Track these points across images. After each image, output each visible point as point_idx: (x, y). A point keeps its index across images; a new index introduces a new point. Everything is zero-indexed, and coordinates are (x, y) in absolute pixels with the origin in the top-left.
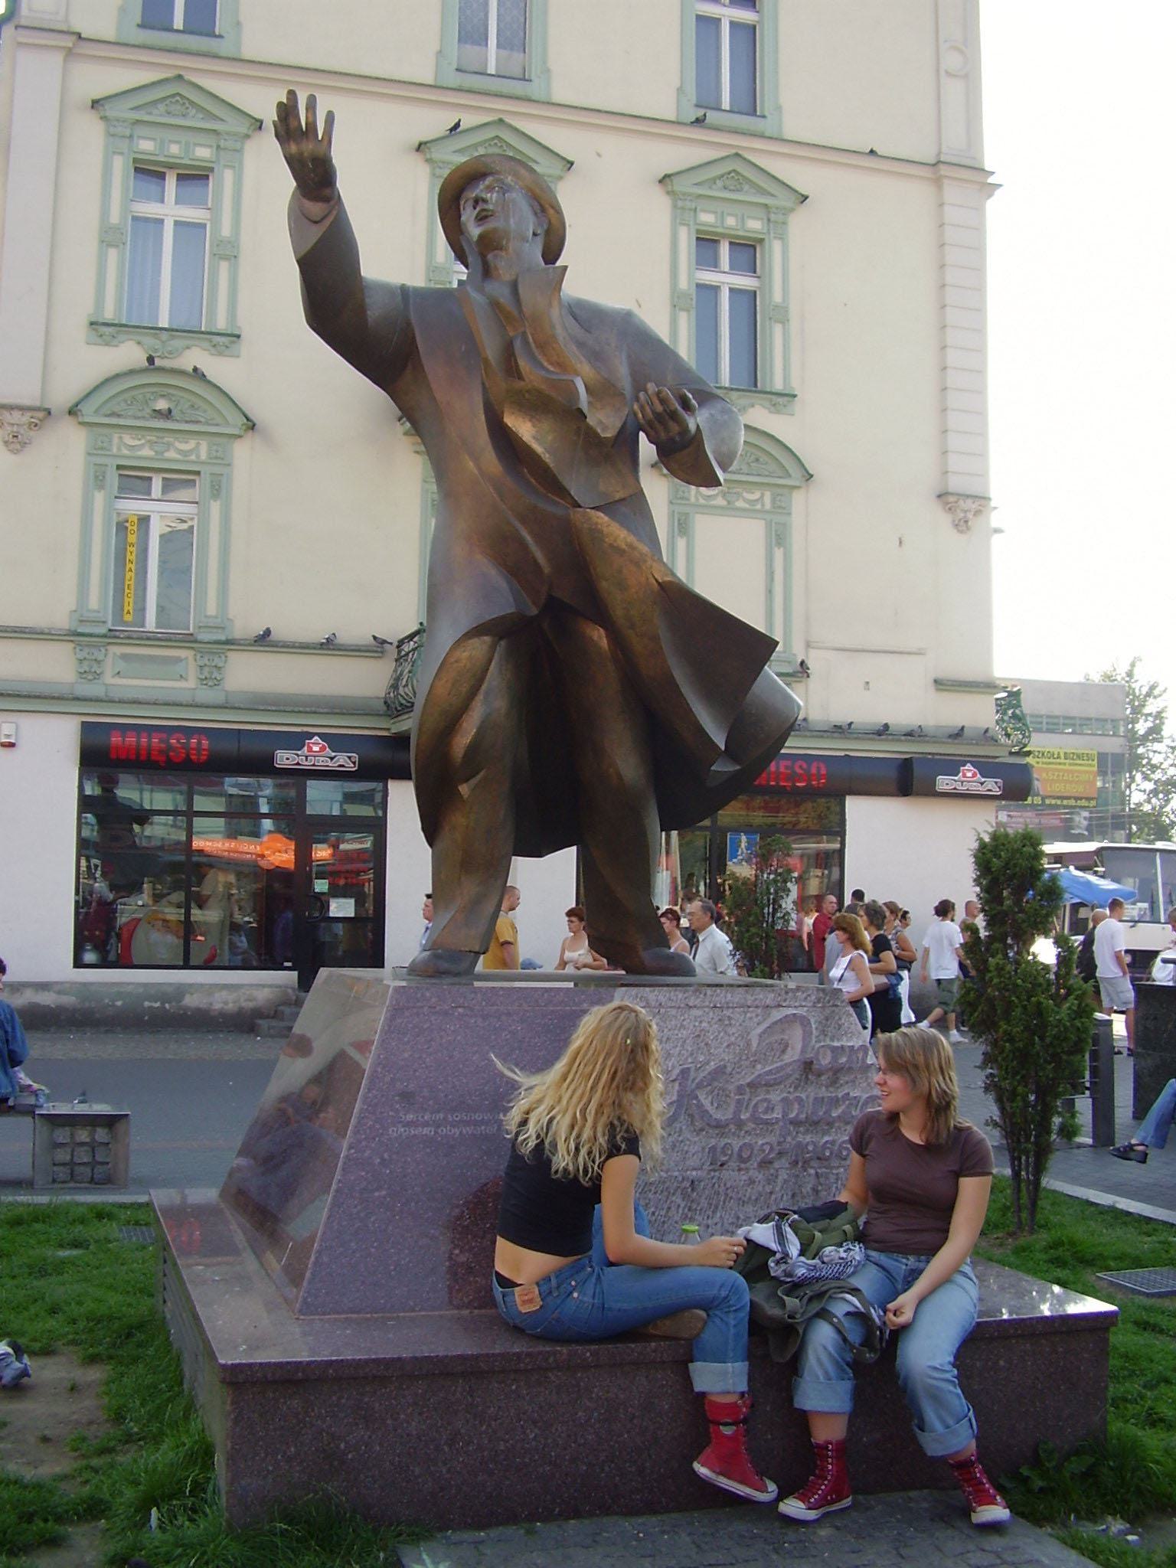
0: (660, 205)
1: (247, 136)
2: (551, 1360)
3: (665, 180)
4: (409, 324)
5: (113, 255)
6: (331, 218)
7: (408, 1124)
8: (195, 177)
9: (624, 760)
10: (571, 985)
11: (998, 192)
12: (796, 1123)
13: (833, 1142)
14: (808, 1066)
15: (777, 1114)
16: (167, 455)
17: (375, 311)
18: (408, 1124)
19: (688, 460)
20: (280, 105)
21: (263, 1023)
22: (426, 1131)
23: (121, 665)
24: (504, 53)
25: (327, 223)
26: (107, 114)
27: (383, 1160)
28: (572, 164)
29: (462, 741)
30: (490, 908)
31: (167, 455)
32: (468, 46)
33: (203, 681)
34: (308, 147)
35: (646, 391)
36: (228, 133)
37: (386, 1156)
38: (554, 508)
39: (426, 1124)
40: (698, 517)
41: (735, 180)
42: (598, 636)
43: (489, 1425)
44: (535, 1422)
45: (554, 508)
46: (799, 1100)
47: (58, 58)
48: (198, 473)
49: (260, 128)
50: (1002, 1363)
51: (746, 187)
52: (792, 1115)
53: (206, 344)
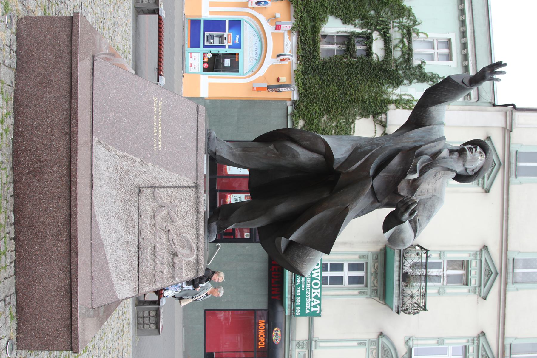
0: (474, 333)
1: (483, 188)
2: (74, 125)
3: (485, 247)
4: (431, 125)
5: (435, 342)
7: (158, 104)
9: (282, 208)
12: (155, 246)
13: (147, 260)
18: (158, 104)
20: (501, 62)
21: (184, 297)
22: (155, 110)
23: (302, 354)
26: (481, 337)
27: (146, 94)
28: (485, 299)
36: (484, 182)
39: (158, 111)
40: (364, 350)
41: (489, 274)
42: (326, 195)
43: (52, 105)
44: (52, 121)
46: (163, 249)
47: (504, 126)
48: (366, 286)
49: (486, 192)
51: (487, 278)
52: (158, 245)
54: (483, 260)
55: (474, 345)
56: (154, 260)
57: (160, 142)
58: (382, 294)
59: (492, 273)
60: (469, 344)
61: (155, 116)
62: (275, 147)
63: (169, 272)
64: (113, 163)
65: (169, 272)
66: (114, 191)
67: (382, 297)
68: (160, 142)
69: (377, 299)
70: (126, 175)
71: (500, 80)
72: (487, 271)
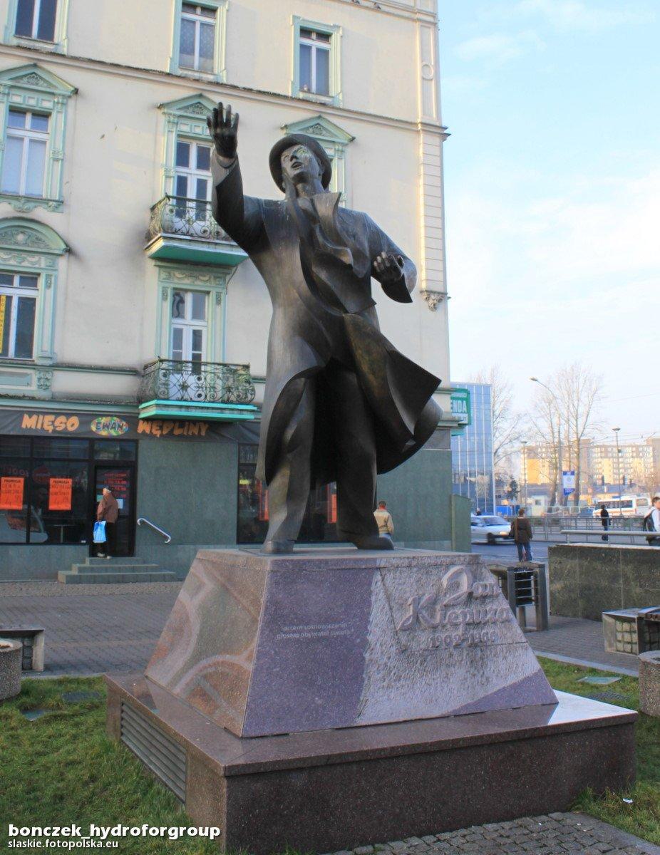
2: (382, 753)
6: (234, 166)
8: (42, 116)
10: (295, 549)
11: (449, 138)
13: (487, 633)
14: (470, 595)
15: (461, 619)
16: (23, 264)
17: (249, 211)
18: (285, 633)
19: (399, 291)
24: (203, 59)
25: (231, 168)
29: (289, 433)
30: (501, 539)
31: (23, 264)
32: (185, 55)
33: (40, 386)
34: (226, 132)
35: (381, 256)
37: (277, 649)
38: (335, 312)
39: (294, 632)
42: (353, 378)
45: (335, 312)
48: (39, 274)
50: (587, 743)
51: (324, 132)
53: (46, 206)
54: (10, 83)
55: (177, 123)
56: (485, 624)
57: (337, 626)
58: (221, 270)
59: (199, 103)
60: (174, 129)
61: (303, 635)
62: (290, 451)
63: (492, 602)
64: (381, 693)
65: (492, 602)
66: (415, 687)
67: (226, 271)
68: (337, 626)
69: (228, 277)
70: (391, 671)
71: (230, 106)
72: (196, 110)
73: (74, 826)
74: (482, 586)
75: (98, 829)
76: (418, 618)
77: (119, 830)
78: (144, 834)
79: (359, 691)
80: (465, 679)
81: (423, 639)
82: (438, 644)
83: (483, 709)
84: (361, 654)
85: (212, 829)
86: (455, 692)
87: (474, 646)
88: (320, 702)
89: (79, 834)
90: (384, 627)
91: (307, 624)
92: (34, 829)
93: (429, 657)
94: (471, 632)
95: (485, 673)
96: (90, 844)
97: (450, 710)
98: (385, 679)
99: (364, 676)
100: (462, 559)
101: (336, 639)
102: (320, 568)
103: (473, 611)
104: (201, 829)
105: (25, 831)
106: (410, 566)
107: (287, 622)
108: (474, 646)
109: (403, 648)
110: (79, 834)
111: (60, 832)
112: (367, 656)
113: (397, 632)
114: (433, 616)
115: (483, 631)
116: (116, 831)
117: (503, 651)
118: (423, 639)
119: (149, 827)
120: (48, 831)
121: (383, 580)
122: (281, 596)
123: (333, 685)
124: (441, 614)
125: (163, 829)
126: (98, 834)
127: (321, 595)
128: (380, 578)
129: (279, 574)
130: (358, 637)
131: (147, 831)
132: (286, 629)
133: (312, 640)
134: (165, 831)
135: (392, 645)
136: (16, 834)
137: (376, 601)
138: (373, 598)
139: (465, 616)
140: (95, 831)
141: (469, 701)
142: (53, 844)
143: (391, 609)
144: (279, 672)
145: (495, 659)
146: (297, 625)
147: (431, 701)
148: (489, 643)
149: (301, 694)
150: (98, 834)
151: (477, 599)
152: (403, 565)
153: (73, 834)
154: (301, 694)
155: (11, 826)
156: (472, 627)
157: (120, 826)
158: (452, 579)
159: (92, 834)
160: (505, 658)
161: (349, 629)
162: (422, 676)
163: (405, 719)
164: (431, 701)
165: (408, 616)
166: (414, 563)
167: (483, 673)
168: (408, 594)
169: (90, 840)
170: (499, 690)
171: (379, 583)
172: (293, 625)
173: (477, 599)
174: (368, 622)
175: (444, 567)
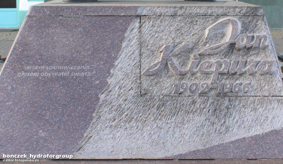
13: (241, 84)
14: (232, 46)
15: (213, 69)
18: (26, 71)
37: (14, 86)
39: (36, 71)
57: (79, 68)
61: (43, 74)
63: (258, 54)
64: (107, 131)
66: (145, 129)
68: (79, 68)
70: (123, 113)
73: (24, 154)
74: (248, 37)
75: (32, 155)
76: (167, 64)
77: (39, 156)
78: (48, 157)
79: (85, 128)
80: (203, 126)
81: (167, 84)
82: (181, 90)
83: (212, 157)
84: (97, 95)
85: (70, 156)
86: (187, 138)
87: (222, 95)
88: (43, 135)
89: (26, 157)
90: (128, 72)
91: (49, 65)
92: (11, 156)
93: (169, 103)
94: (223, 81)
95: (227, 122)
96: (30, 160)
97: (177, 153)
98: (115, 120)
99: (94, 115)
100: (238, 10)
101: (75, 80)
102: (77, 14)
103: (230, 62)
104: (66, 155)
105: (8, 156)
106: (174, 16)
107: (31, 62)
108: (222, 95)
109: (143, 92)
110: (26, 157)
111: (20, 156)
112: (102, 97)
113: (140, 76)
114: (184, 64)
115: (237, 82)
116: (38, 156)
117: (254, 103)
118: (167, 84)
119: (49, 155)
120: (16, 156)
121: (140, 28)
122: (31, 39)
123: (60, 120)
124: (193, 62)
125: (54, 155)
126: (32, 157)
127: (71, 39)
128: (137, 25)
129: (34, 19)
130: (97, 79)
131: (49, 156)
132: (28, 68)
133: (51, 79)
134: (55, 156)
135: (132, 88)
136: (5, 157)
137: (127, 46)
138: (124, 44)
139: (221, 65)
140: (32, 156)
141: (200, 148)
142: (17, 160)
143: (141, 55)
144: (11, 105)
145: (243, 109)
146: (39, 65)
147: (158, 144)
148: (240, 94)
149: (27, 126)
150: (32, 157)
151: (239, 50)
152: (168, 14)
153: (24, 157)
154: (27, 126)
155: (4, 154)
156: (225, 77)
157: (40, 154)
158: (217, 29)
159: (30, 157)
160: (255, 110)
161: (91, 71)
162: (155, 119)
163: (125, 158)
164: (158, 144)
165: (157, 61)
166: (180, 12)
167: (225, 122)
168: (163, 42)
169: (30, 159)
170: (237, 140)
171: (135, 30)
172: (36, 65)
173: (239, 50)
174: (112, 66)
175: (213, 17)
